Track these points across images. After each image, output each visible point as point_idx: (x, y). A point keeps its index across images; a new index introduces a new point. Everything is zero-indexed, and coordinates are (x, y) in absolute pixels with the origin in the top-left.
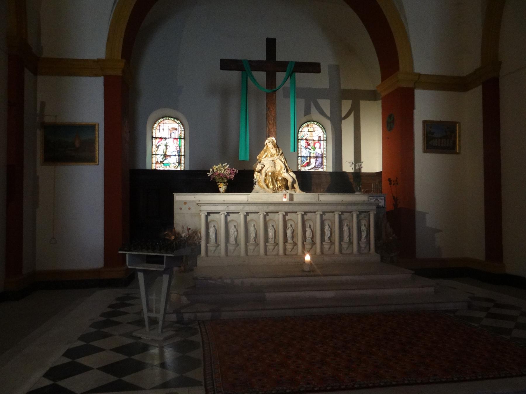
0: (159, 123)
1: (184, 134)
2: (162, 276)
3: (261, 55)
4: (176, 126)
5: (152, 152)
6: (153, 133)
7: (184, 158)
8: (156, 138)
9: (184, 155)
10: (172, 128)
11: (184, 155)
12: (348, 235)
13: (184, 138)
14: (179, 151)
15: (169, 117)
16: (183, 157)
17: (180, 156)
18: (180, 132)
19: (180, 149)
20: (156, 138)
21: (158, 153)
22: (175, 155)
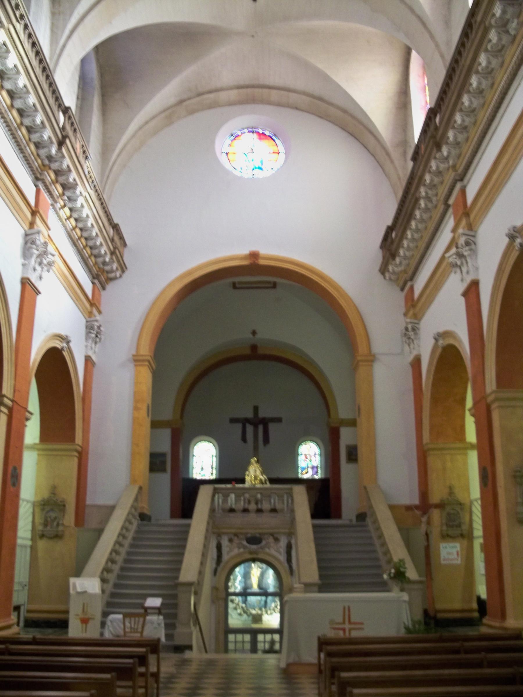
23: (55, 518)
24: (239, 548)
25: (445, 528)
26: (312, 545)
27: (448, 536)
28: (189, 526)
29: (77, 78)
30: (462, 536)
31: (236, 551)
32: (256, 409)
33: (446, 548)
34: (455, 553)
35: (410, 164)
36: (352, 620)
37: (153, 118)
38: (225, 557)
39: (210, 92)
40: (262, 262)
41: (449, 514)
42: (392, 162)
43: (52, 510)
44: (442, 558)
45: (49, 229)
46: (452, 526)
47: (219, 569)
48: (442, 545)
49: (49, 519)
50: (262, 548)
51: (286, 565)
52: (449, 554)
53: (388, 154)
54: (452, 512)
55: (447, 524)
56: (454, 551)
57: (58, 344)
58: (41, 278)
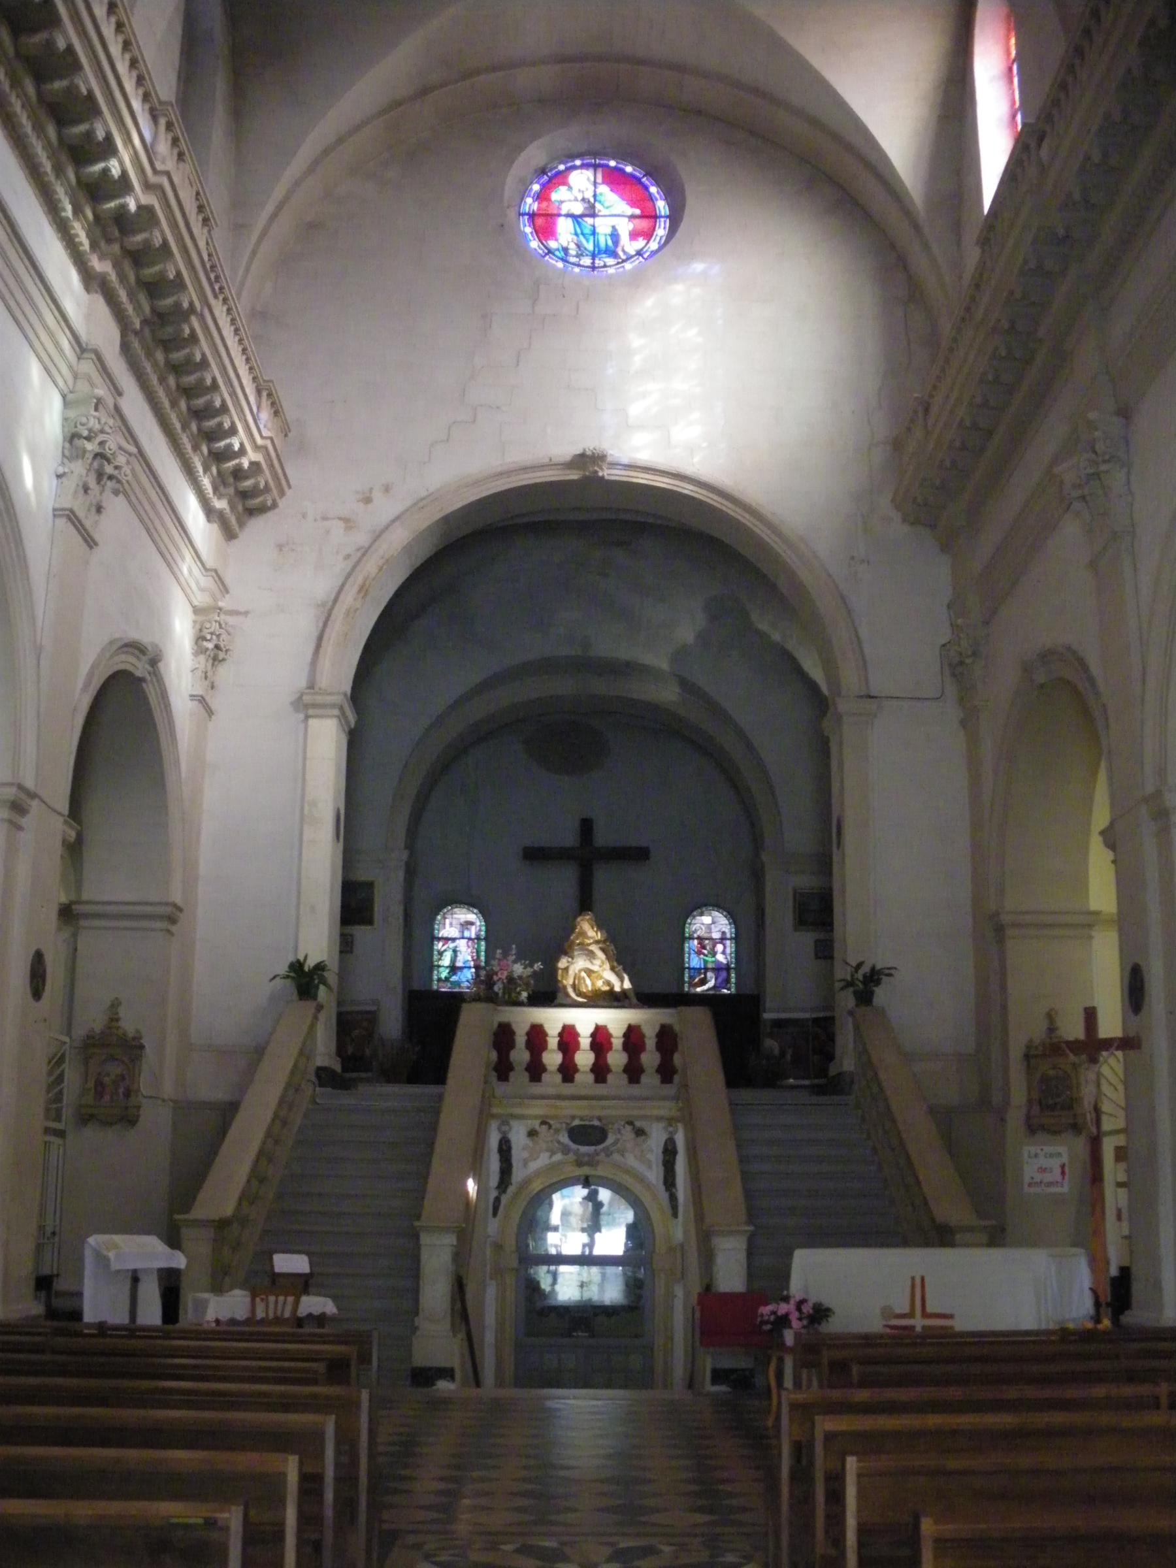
3: (570, 839)
23: (123, 1078)
24: (553, 1153)
25: (1036, 1109)
26: (205, 1186)
27: (1043, 1128)
28: (440, 1097)
29: (178, 30)
30: (1076, 1128)
31: (543, 1160)
32: (586, 827)
33: (1036, 1155)
34: (1058, 1171)
35: (972, 256)
36: (929, 1309)
37: (357, 128)
38: (518, 1175)
39: (494, 69)
40: (607, 473)
41: (1044, 1079)
42: (926, 247)
43: (112, 1058)
44: (1027, 1180)
45: (120, 394)
46: (1052, 1108)
47: (504, 1199)
48: (1028, 1149)
49: (106, 1080)
50: (608, 1153)
51: (664, 1196)
52: (1043, 1170)
53: (917, 227)
54: (1051, 1073)
55: (1040, 1103)
56: (1055, 1164)
57: (126, 662)
58: (99, 509)
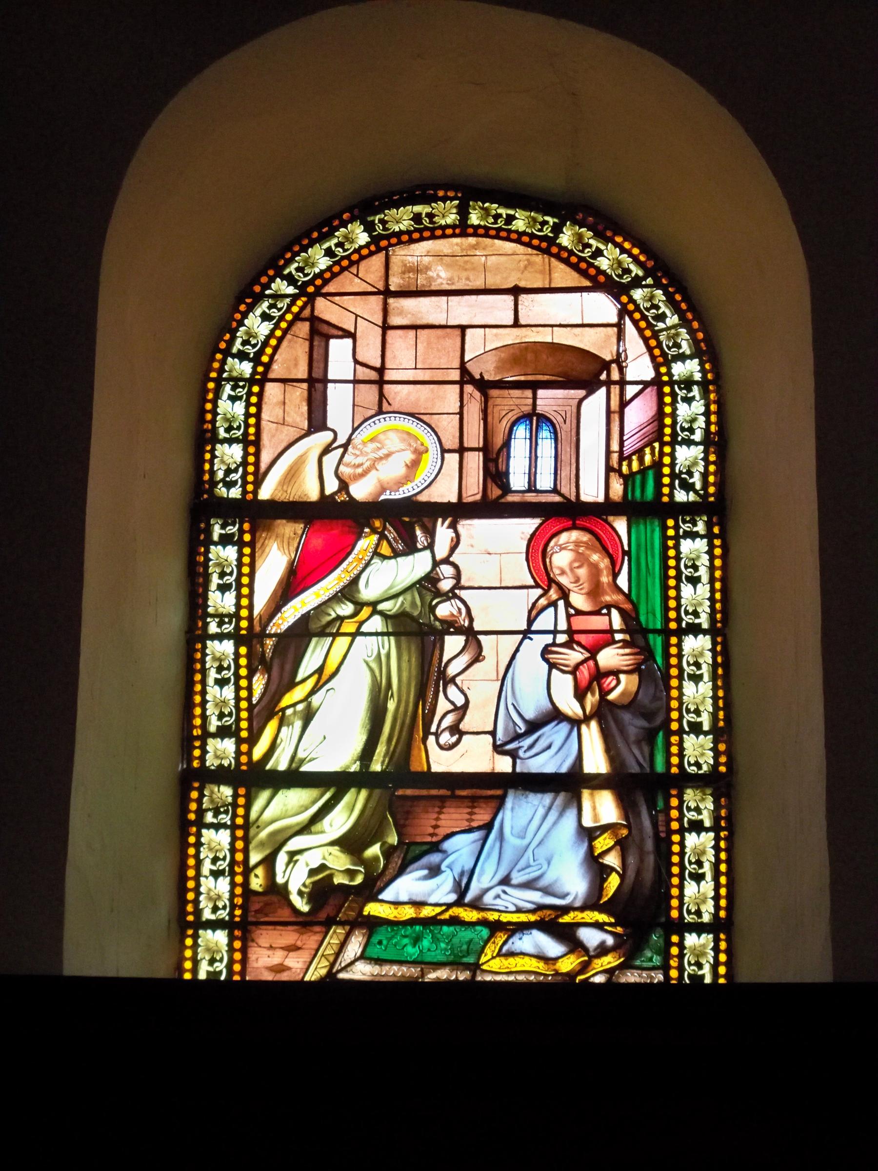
0: (312, 290)
1: (717, 443)
2: (500, 803)
4: (579, 316)
5: (189, 738)
6: (204, 438)
7: (726, 826)
8: (258, 516)
9: (715, 782)
10: (521, 354)
11: (715, 782)
12: (612, 425)
13: (717, 509)
14: (639, 721)
15: (469, 193)
16: (700, 804)
17: (643, 787)
18: (638, 414)
19: (656, 675)
20: (258, 516)
21: (281, 746)
22: (570, 784)
